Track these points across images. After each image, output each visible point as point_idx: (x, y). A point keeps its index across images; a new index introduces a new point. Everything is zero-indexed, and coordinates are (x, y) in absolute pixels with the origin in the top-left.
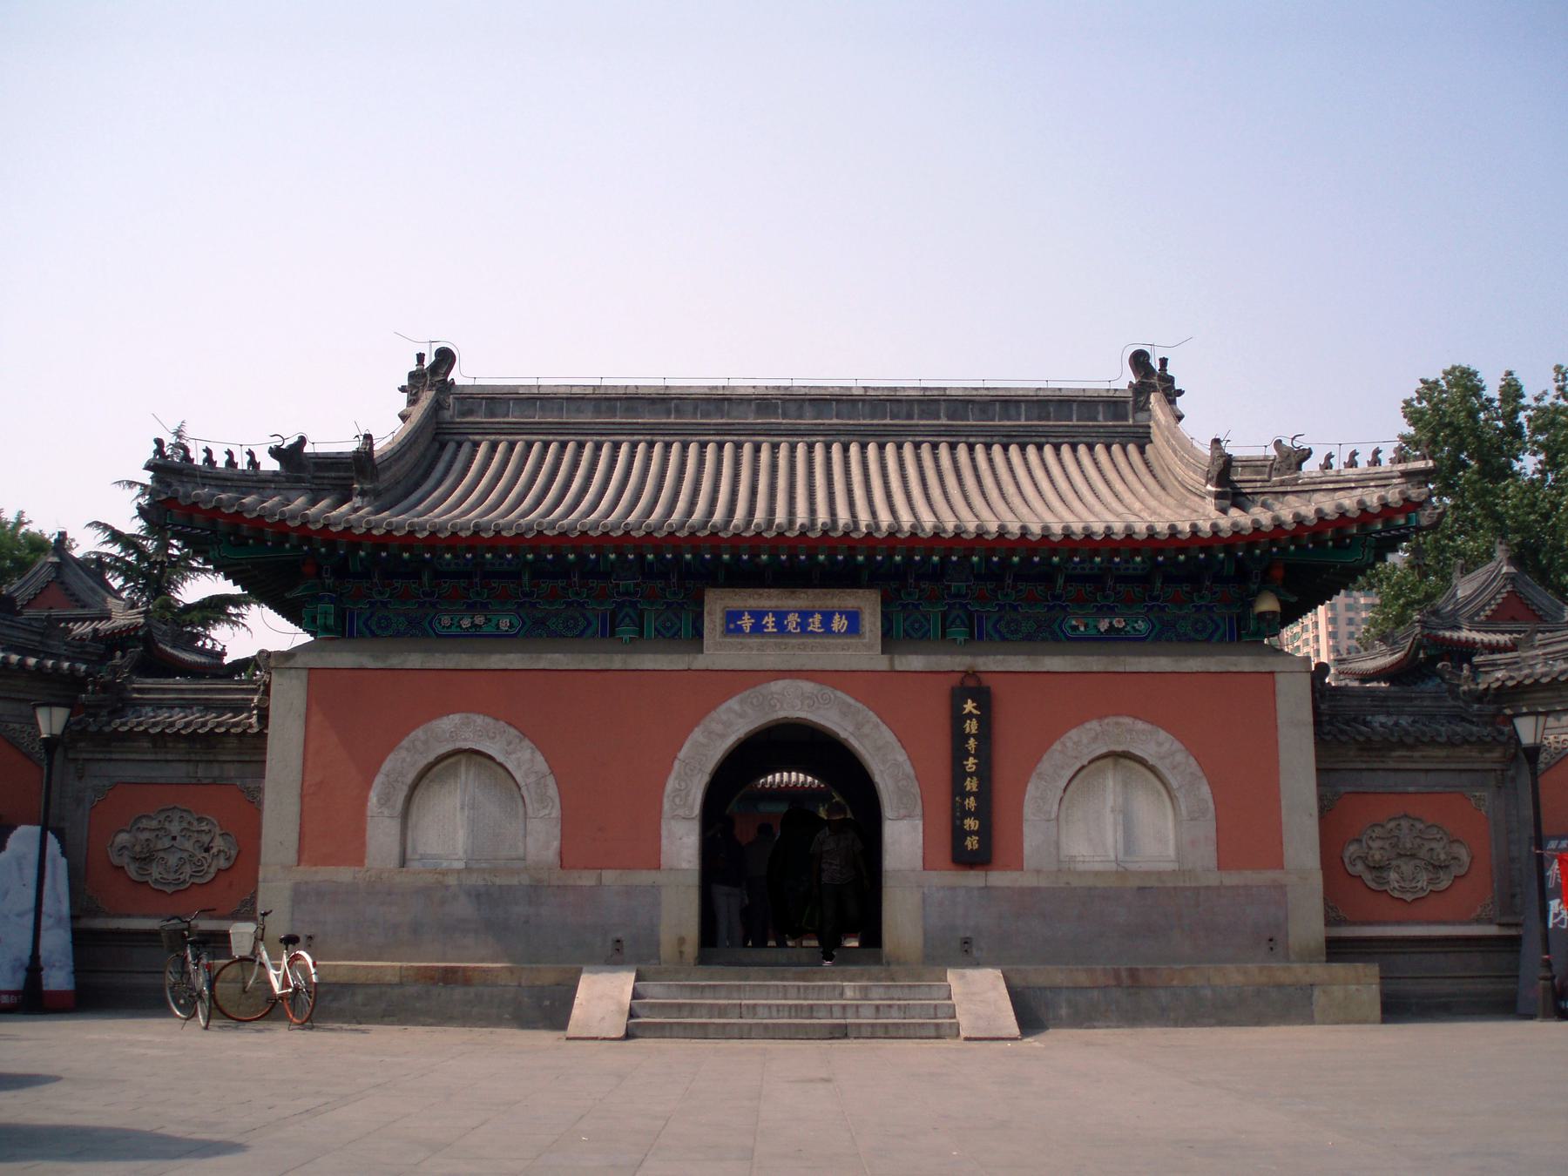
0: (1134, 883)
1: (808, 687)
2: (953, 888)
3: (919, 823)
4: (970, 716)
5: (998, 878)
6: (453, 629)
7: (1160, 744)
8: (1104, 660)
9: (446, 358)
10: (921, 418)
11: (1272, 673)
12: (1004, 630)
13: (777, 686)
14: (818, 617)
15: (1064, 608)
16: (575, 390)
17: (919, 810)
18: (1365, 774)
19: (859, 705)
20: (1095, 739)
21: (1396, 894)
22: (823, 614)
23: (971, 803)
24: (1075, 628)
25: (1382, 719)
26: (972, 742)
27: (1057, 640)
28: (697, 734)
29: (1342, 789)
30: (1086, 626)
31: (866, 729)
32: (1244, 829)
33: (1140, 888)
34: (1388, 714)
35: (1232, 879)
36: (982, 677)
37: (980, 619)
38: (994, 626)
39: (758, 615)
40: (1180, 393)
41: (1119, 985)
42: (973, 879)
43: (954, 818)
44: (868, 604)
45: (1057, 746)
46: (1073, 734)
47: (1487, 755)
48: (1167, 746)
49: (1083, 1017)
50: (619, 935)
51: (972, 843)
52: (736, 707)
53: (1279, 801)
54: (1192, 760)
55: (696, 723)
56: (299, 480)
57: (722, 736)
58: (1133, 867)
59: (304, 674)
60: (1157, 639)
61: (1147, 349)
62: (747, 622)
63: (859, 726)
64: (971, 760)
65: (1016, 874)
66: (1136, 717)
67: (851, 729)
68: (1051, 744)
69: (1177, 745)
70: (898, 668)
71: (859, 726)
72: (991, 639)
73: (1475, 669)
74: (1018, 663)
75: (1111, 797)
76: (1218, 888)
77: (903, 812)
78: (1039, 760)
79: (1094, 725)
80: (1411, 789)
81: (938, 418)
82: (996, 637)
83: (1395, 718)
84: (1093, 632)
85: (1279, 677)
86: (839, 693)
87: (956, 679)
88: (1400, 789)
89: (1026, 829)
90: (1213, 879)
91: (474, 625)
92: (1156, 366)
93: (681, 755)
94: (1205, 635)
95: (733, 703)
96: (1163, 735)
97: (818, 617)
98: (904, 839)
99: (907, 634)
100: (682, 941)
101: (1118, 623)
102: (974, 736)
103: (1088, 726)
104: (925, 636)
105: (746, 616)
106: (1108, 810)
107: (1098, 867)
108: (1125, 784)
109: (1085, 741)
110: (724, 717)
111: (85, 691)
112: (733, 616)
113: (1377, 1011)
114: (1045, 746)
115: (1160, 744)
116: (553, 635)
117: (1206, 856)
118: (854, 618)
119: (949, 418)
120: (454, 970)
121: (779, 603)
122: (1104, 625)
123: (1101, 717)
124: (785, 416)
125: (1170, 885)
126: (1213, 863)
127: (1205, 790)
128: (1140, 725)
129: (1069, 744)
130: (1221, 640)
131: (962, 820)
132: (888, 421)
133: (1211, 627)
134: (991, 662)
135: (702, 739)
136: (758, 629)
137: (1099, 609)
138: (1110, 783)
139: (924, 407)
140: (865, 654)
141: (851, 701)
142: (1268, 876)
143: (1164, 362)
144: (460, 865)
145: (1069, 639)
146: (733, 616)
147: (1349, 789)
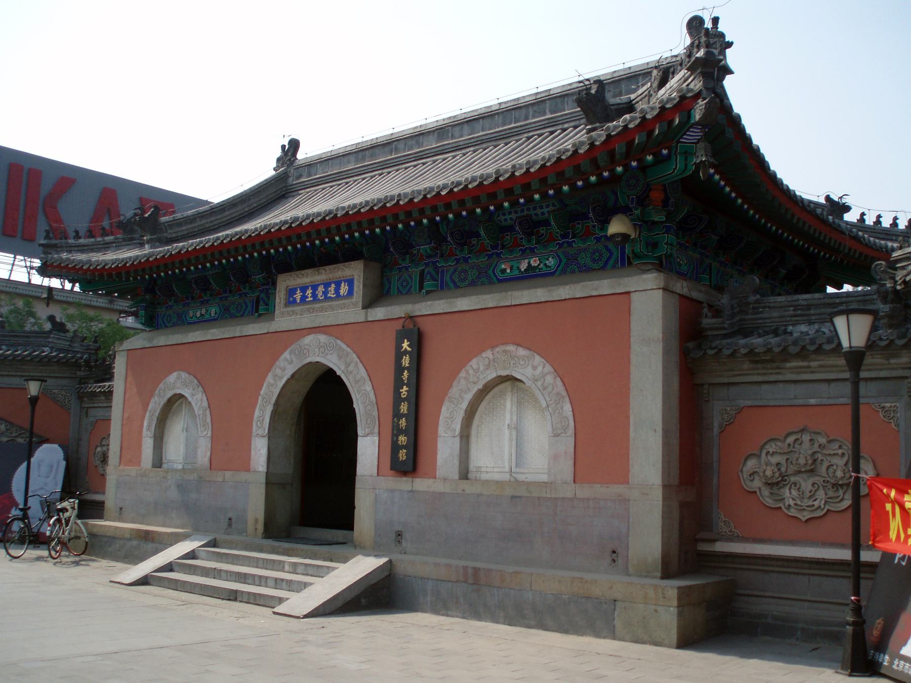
0: (509, 492)
1: (323, 338)
2: (392, 491)
3: (376, 439)
4: (406, 352)
5: (421, 484)
6: (194, 318)
7: (535, 368)
8: (497, 296)
9: (294, 145)
10: (534, 117)
11: (628, 293)
12: (457, 280)
13: (308, 340)
14: (333, 286)
15: (498, 255)
16: (348, 149)
17: (376, 430)
18: (765, 387)
19: (349, 350)
20: (488, 367)
21: (793, 512)
22: (335, 283)
23: (403, 422)
24: (504, 271)
25: (804, 328)
26: (406, 373)
27: (491, 283)
28: (270, 378)
29: (742, 403)
30: (511, 268)
31: (351, 368)
32: (597, 447)
33: (513, 497)
34: (810, 323)
35: (584, 491)
36: (418, 319)
37: (443, 272)
38: (451, 277)
39: (304, 289)
40: (730, 45)
41: (466, 582)
42: (404, 484)
43: (393, 434)
44: (355, 270)
45: (463, 374)
46: (474, 363)
47: (893, 361)
48: (540, 369)
49: (441, 607)
50: (230, 515)
51: (402, 455)
52: (288, 357)
53: (628, 417)
54: (559, 382)
55: (269, 370)
56: (132, 239)
57: (281, 378)
58: (521, 478)
59: (126, 353)
60: (564, 272)
61: (700, 14)
62: (298, 296)
63: (348, 365)
64: (405, 388)
65: (431, 481)
66: (519, 345)
67: (343, 368)
68: (459, 372)
69: (548, 368)
70: (370, 319)
71: (348, 365)
72: (449, 289)
73: (892, 265)
74: (439, 306)
75: (508, 416)
76: (571, 500)
77: (367, 430)
78: (450, 387)
79: (488, 354)
80: (812, 401)
81: (545, 114)
82: (451, 285)
83: (816, 326)
84: (516, 272)
85: (634, 297)
86: (339, 342)
87: (398, 325)
88: (801, 402)
89: (440, 445)
90: (568, 491)
91: (202, 315)
92: (708, 25)
93: (262, 392)
94: (601, 264)
95: (286, 355)
96: (538, 359)
97: (333, 286)
98: (369, 450)
99: (400, 292)
100: (256, 520)
101: (534, 262)
102: (407, 368)
103: (484, 355)
104: (409, 292)
105: (299, 291)
106: (506, 427)
107: (497, 477)
108: (520, 404)
109: (482, 368)
110: (282, 365)
111: (80, 370)
112: (291, 292)
113: (674, 636)
114: (454, 375)
115: (535, 368)
116: (233, 316)
117: (566, 467)
118: (350, 283)
119: (552, 112)
120: (147, 533)
121: (312, 279)
122: (524, 266)
123: (493, 347)
124: (453, 137)
125: (535, 495)
126: (570, 477)
127: (567, 408)
128: (522, 352)
129: (471, 371)
130: (614, 267)
131: (397, 436)
132: (513, 125)
133: (606, 255)
134: (424, 308)
135: (272, 381)
136: (303, 298)
137: (523, 251)
138: (508, 404)
139: (536, 108)
140: (351, 312)
141: (344, 346)
142: (617, 489)
143: (715, 21)
144: (180, 467)
145: (500, 281)
146: (291, 292)
147: (749, 403)
